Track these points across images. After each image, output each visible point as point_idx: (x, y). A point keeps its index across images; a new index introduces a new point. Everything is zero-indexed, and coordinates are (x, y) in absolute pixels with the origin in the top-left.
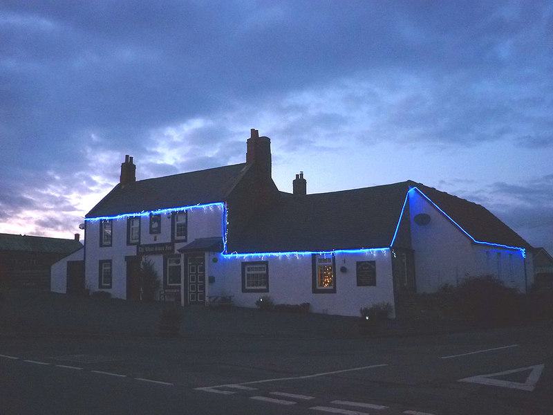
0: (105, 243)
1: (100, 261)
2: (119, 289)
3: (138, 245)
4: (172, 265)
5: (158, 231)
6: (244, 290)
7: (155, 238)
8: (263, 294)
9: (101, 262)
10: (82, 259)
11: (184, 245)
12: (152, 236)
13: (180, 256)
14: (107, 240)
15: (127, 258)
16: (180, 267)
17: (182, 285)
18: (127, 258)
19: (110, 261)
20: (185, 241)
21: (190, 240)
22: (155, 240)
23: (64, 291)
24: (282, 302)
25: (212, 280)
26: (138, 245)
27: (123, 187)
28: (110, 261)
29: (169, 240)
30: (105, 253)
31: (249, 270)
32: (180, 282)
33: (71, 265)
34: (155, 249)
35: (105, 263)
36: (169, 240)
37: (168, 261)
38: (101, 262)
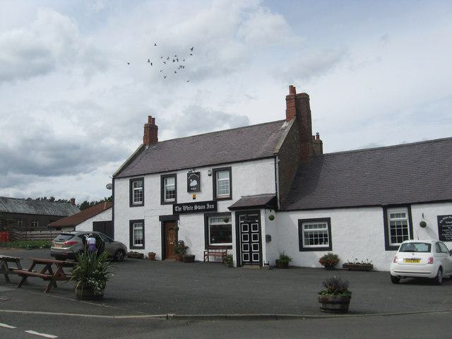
0: (135, 203)
1: (300, 251)
2: (153, 244)
3: (175, 204)
4: (213, 224)
5: (198, 189)
6: (302, 249)
7: (194, 196)
8: (326, 253)
9: (132, 223)
12: (191, 196)
13: (230, 214)
14: (171, 196)
15: (162, 218)
17: (234, 244)
18: (162, 218)
19: (142, 222)
20: (230, 198)
22: (194, 198)
24: (352, 260)
25: (269, 238)
27: (147, 147)
28: (142, 222)
29: (211, 199)
30: (137, 213)
31: (306, 227)
33: (97, 225)
34: (191, 209)
35: (136, 224)
36: (211, 199)
37: (303, 226)
38: (132, 223)
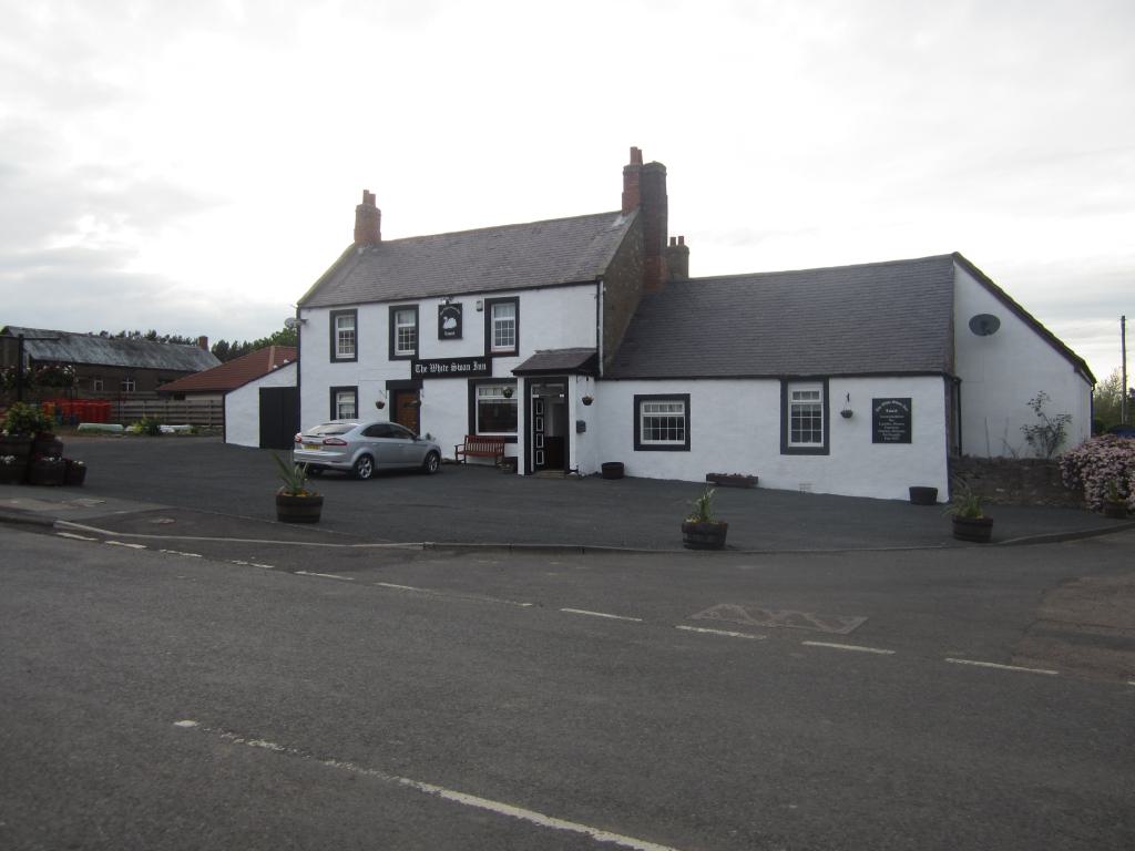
3: (415, 360)
5: (457, 334)
6: (638, 447)
9: (335, 392)
10: (294, 384)
11: (514, 363)
15: (390, 385)
16: (793, 428)
18: (390, 385)
20: (516, 353)
21: (527, 352)
23: (255, 442)
24: (646, 474)
25: (581, 427)
26: (415, 360)
29: (481, 353)
30: (343, 375)
32: (514, 427)
36: (481, 353)
